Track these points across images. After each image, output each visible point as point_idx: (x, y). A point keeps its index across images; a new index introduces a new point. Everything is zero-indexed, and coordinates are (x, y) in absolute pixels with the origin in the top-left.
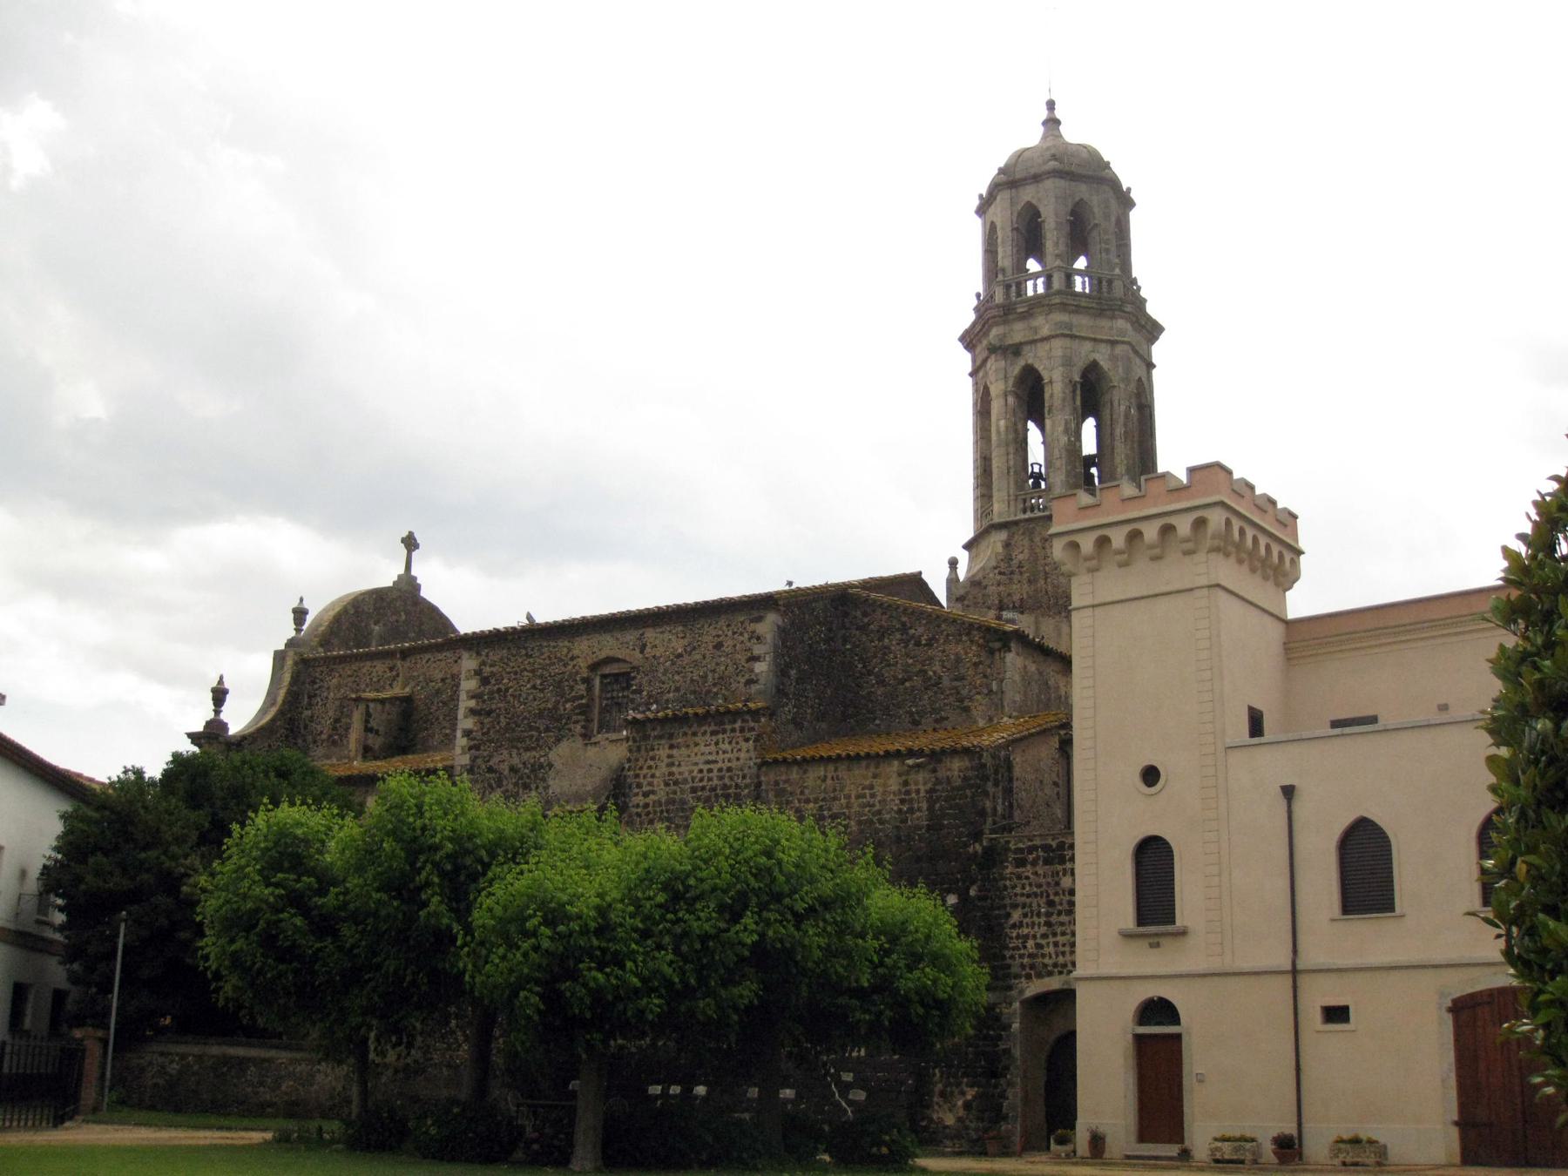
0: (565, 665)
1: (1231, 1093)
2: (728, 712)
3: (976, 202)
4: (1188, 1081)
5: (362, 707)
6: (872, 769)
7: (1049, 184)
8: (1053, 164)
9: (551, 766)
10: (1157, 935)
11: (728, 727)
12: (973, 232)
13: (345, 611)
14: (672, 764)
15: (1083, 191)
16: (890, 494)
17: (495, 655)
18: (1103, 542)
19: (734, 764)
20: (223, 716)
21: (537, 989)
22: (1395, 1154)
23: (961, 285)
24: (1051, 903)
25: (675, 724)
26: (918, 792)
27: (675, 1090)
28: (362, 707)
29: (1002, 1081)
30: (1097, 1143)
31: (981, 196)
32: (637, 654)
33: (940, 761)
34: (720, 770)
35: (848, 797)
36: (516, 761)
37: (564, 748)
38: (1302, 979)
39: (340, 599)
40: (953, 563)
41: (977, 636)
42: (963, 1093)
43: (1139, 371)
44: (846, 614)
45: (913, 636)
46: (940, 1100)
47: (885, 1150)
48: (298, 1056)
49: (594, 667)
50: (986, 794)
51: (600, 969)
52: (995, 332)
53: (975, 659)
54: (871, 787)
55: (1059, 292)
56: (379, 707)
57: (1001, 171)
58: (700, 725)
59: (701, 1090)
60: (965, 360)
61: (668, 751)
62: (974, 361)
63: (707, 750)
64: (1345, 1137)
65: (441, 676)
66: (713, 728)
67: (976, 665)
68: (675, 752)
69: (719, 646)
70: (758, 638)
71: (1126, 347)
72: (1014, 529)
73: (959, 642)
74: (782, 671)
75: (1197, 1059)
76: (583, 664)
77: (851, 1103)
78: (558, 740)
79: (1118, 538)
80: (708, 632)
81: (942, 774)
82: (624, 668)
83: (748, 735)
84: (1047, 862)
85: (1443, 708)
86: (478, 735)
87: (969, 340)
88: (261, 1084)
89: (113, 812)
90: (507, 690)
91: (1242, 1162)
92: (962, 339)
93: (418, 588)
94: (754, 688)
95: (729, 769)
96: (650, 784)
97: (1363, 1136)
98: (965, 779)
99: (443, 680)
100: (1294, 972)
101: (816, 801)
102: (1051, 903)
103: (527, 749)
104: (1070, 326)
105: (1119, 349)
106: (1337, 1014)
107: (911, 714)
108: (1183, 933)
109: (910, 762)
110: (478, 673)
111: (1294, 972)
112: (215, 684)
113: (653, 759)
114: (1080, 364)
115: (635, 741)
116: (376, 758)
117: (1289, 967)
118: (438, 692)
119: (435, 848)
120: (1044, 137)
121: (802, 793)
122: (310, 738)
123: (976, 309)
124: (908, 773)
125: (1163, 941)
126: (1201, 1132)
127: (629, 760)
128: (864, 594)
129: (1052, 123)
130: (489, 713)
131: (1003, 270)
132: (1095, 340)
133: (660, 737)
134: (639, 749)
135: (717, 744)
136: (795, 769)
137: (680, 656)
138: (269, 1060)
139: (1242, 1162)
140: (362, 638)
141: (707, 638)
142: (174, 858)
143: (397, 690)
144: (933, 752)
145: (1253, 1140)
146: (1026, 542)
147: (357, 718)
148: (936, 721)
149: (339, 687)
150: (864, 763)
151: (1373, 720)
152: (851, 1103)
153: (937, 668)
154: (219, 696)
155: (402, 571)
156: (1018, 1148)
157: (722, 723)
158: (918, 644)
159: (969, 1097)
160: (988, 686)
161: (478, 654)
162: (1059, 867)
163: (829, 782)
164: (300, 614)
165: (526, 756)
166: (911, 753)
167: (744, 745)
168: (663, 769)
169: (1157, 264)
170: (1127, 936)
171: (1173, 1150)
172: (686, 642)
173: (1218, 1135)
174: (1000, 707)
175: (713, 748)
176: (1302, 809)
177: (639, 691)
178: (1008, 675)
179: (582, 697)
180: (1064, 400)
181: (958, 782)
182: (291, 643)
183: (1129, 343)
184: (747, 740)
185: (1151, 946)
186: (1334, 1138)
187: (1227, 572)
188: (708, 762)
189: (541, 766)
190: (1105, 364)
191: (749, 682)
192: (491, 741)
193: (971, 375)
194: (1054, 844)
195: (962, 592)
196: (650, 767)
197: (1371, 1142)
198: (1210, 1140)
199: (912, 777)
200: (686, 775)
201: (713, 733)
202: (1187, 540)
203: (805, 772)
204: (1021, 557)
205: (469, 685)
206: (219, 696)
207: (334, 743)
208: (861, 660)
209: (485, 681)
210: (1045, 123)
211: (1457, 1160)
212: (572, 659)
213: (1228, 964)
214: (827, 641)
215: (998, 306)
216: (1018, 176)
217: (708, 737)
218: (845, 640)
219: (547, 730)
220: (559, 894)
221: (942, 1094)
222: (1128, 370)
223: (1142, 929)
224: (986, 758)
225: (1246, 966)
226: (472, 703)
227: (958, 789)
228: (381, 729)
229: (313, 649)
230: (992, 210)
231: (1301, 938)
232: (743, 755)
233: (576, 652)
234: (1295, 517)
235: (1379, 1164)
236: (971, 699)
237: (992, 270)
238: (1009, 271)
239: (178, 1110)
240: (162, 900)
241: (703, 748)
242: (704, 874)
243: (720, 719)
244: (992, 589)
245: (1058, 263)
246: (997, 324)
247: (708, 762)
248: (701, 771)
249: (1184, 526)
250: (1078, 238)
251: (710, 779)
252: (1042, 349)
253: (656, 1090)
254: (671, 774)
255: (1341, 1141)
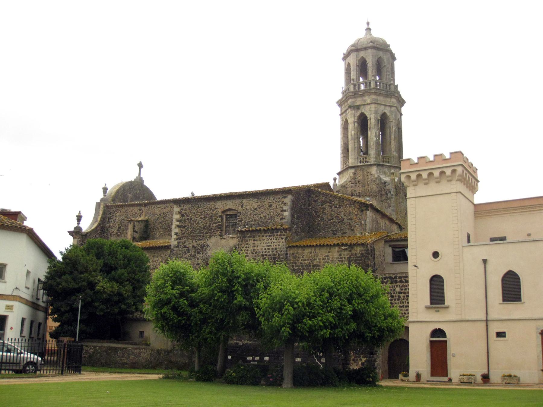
0: (213, 211)
1: (464, 359)
2: (276, 229)
3: (342, 56)
4: (449, 356)
5: (132, 223)
6: (328, 250)
7: (370, 51)
8: (371, 44)
9: (208, 246)
10: (438, 308)
11: (275, 234)
12: (341, 67)
13: (120, 189)
14: (255, 246)
15: (381, 54)
16: (310, 154)
17: (187, 206)
18: (419, 176)
19: (277, 247)
20: (81, 225)
21: (288, 326)
22: (522, 380)
23: (337, 85)
24: (392, 297)
25: (255, 233)
26: (345, 258)
27: (257, 358)
28: (132, 223)
29: (375, 356)
30: (418, 377)
31: (344, 54)
32: (240, 208)
33: (352, 248)
34: (273, 249)
35: (320, 259)
36: (195, 244)
37: (213, 240)
38: (489, 323)
39: (118, 185)
40: (335, 179)
41: (357, 205)
42: (361, 360)
43: (399, 116)
44: (309, 196)
45: (334, 205)
46: (353, 362)
47: (371, 379)
48: (135, 347)
49: (223, 212)
50: (369, 259)
51: (310, 320)
52: (349, 100)
53: (356, 213)
54: (328, 256)
55: (373, 88)
56: (138, 224)
57: (352, 46)
58: (265, 233)
59: (267, 358)
60: (338, 110)
61: (253, 242)
62: (341, 110)
63: (268, 242)
64: (507, 374)
65: (159, 213)
66: (269, 234)
67: (356, 215)
68: (255, 242)
69: (270, 206)
70: (285, 204)
71: (395, 108)
72: (357, 168)
73: (350, 207)
74: (293, 215)
75: (452, 349)
76: (220, 211)
77: (322, 363)
78: (210, 237)
79: (425, 175)
80: (267, 201)
81: (353, 252)
82: (235, 212)
83: (283, 237)
84: (392, 282)
85: (529, 235)
86: (180, 234)
87: (340, 103)
88: (123, 357)
89: (70, 260)
90: (191, 219)
91: (471, 383)
92: (337, 103)
93: (143, 181)
94: (284, 221)
95: (276, 249)
96: (246, 253)
97: (513, 374)
98: (362, 254)
99: (160, 215)
100: (487, 320)
101: (308, 260)
102: (392, 297)
103: (199, 240)
104: (377, 100)
105: (393, 109)
106: (501, 335)
107: (333, 231)
108: (447, 307)
109: (343, 248)
110: (180, 213)
111: (487, 320)
112: (77, 214)
113: (247, 244)
114: (380, 113)
115: (240, 238)
116: (137, 241)
117: (485, 319)
118: (158, 219)
119: (239, 277)
120: (366, 34)
121: (303, 257)
122: (109, 234)
123: (343, 93)
124: (341, 251)
125: (440, 310)
126: (455, 371)
127: (238, 245)
128: (317, 189)
129: (368, 30)
130: (184, 227)
131: (353, 80)
132: (385, 105)
133: (250, 237)
134: (242, 241)
135: (271, 240)
136: (300, 249)
137: (256, 209)
138: (126, 348)
139: (471, 383)
140: (125, 199)
141: (265, 203)
142: (93, 276)
143: (142, 218)
144: (351, 244)
145: (474, 376)
146: (361, 173)
147: (130, 226)
148: (342, 234)
149: (120, 216)
150: (325, 248)
151: (504, 239)
152: (322, 363)
153: (342, 215)
154: (79, 218)
155: (137, 175)
156: (381, 378)
157: (273, 233)
158: (336, 207)
159: (363, 361)
160: (361, 223)
161: (180, 206)
162: (395, 284)
163: (312, 254)
164: (105, 190)
165: (198, 242)
166: (343, 245)
167: (281, 241)
168: (251, 248)
169: (403, 79)
170: (427, 308)
171: (446, 379)
172: (258, 204)
173: (462, 374)
174: (365, 230)
175: (270, 241)
176: (488, 266)
177: (241, 221)
178: (368, 219)
179: (219, 222)
180: (375, 125)
181: (359, 255)
182: (102, 200)
183: (396, 107)
184: (282, 239)
185: (436, 311)
186: (501, 375)
187: (460, 187)
188: (268, 246)
189: (204, 246)
190: (388, 114)
191: (282, 219)
192: (185, 237)
193: (340, 115)
194: (393, 276)
195: (338, 189)
196: (246, 247)
197: (515, 376)
198: (459, 375)
199: (343, 253)
200: (260, 250)
201: (269, 236)
202: (449, 177)
203: (304, 250)
204: (359, 178)
205: (177, 217)
206: (79, 218)
207: (118, 236)
208: (315, 212)
209: (183, 216)
210: (366, 29)
211: (415, 380)
212: (216, 209)
213: (464, 318)
214: (305, 205)
215: (352, 92)
216: (359, 47)
217: (268, 237)
218: (309, 205)
219: (206, 233)
220: (293, 294)
221: (354, 360)
222: (396, 115)
223: (433, 306)
224: (369, 247)
225: (470, 319)
226: (178, 223)
227: (359, 257)
228: (138, 231)
229: (109, 202)
230: (349, 58)
231: (489, 309)
232: (281, 244)
233: (217, 206)
234: (477, 170)
235: (518, 384)
236: (355, 226)
237: (348, 79)
238: (355, 80)
239: (93, 366)
240: (89, 291)
241: (266, 241)
242: (339, 288)
243: (273, 231)
244: (349, 189)
245: (373, 78)
246: (351, 98)
247: (268, 246)
248: (265, 249)
249: (448, 172)
250: (379, 70)
251: (269, 252)
252: (368, 107)
253: (250, 358)
254: (254, 250)
255: (504, 376)
